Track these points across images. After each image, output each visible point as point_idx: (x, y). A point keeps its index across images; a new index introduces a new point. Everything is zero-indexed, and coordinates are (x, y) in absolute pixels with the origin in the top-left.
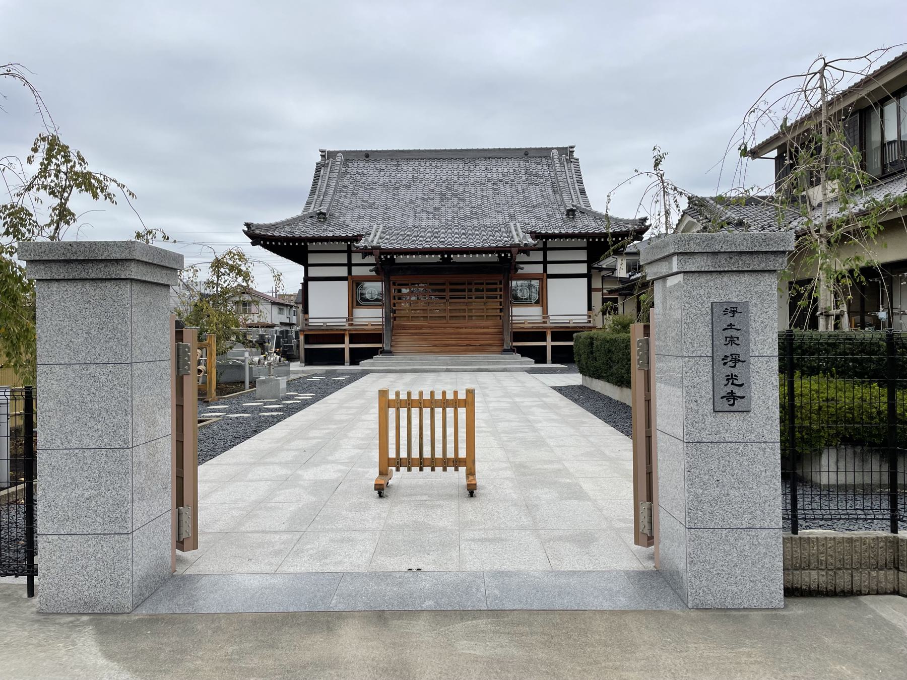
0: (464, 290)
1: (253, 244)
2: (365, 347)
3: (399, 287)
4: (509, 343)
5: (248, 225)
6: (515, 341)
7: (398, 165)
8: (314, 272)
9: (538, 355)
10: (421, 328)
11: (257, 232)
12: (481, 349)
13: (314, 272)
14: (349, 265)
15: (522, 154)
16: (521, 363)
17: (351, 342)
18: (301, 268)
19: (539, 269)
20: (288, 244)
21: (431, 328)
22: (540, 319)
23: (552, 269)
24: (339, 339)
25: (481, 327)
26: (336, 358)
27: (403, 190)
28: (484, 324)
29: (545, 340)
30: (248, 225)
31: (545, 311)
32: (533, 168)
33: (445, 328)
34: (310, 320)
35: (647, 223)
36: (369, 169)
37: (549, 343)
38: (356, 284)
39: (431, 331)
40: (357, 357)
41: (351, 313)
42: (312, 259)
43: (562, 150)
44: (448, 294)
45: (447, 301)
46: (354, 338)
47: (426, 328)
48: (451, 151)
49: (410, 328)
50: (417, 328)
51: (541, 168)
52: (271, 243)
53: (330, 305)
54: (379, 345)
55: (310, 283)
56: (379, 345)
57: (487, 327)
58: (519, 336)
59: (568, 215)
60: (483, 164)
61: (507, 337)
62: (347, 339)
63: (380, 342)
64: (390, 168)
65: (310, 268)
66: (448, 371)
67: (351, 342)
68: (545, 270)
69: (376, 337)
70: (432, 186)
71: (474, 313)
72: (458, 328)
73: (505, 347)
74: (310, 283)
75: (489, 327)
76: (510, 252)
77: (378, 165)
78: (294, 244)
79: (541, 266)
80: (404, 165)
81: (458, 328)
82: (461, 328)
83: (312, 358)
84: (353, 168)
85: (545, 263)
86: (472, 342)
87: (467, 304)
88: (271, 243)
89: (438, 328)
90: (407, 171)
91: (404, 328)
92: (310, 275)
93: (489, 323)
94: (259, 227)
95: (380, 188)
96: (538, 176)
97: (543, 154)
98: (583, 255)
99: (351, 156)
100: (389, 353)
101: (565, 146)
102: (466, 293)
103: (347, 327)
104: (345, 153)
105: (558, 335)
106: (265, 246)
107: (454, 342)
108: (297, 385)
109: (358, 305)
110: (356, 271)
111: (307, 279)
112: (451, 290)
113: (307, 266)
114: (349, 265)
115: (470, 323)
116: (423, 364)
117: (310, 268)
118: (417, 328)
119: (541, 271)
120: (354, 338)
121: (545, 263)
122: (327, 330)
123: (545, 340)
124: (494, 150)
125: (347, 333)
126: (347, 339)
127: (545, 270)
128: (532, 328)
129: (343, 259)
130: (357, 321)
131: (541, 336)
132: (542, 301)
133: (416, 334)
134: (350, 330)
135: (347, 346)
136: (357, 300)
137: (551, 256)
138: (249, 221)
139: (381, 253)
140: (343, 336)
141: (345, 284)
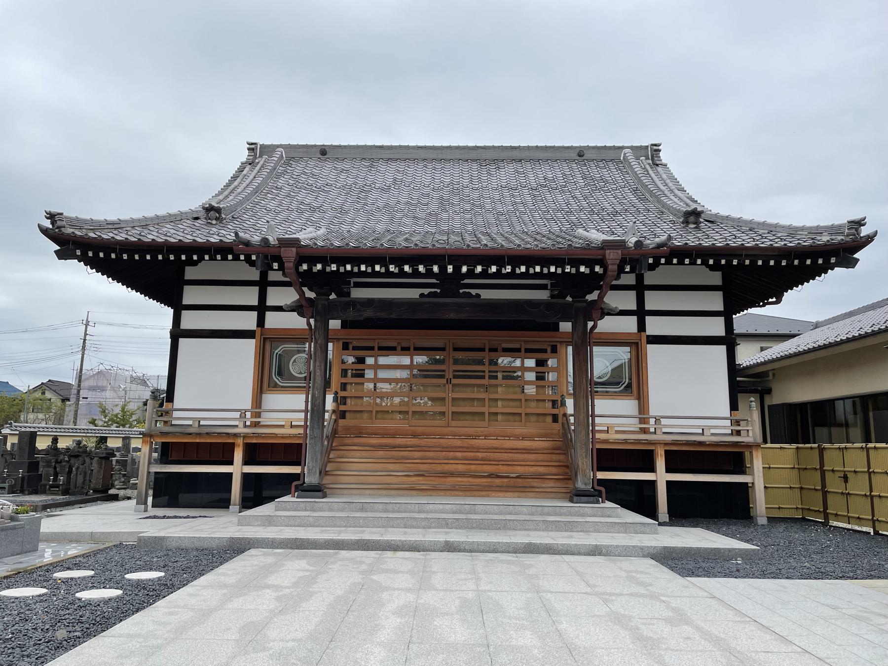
0: (480, 362)
1: (62, 255)
2: (273, 472)
3: (360, 353)
4: (588, 475)
5: (51, 216)
6: (600, 469)
7: (372, 166)
8: (190, 321)
9: (639, 499)
10: (393, 436)
11: (69, 231)
12: (520, 485)
13: (190, 321)
14: (262, 309)
15: (574, 155)
16: (626, 528)
17: (247, 462)
18: (168, 312)
19: (629, 324)
20: (131, 257)
21: (415, 435)
22: (633, 424)
23: (654, 326)
24: (224, 454)
25: (517, 438)
26: (211, 494)
27: (374, 195)
28: (519, 430)
29: (652, 469)
30: (51, 216)
31: (643, 408)
32: (595, 172)
33: (442, 436)
34: (176, 414)
35: (865, 231)
36: (327, 171)
37: (661, 476)
38: (268, 341)
39: (414, 441)
40: (258, 492)
41: (257, 402)
42: (191, 295)
43: (638, 150)
44: (450, 369)
45: (449, 381)
46: (254, 454)
47: (404, 435)
48: (458, 148)
49: (371, 434)
50: (384, 434)
51: (610, 173)
52: (96, 254)
53: (220, 387)
54: (296, 470)
55: (182, 341)
56: (296, 470)
57: (531, 438)
58: (609, 458)
59: (686, 222)
60: (510, 168)
61: (584, 462)
62: (238, 455)
63: (297, 463)
64: (359, 173)
65: (185, 314)
66: (450, 547)
67: (247, 462)
68: (642, 326)
69: (291, 452)
70: (426, 191)
71: (500, 407)
72: (469, 436)
73: (580, 485)
74: (182, 341)
75: (530, 439)
76: (602, 262)
77: (340, 166)
78: (143, 257)
79: (634, 319)
80: (382, 167)
81: (469, 436)
82: (476, 437)
83: (171, 493)
84: (298, 168)
85: (641, 313)
86: (503, 469)
87: (486, 388)
88: (96, 254)
89: (428, 435)
90: (387, 173)
91: (359, 433)
92: (185, 324)
93: (530, 428)
94: (76, 223)
95: (336, 191)
96: (606, 182)
97: (609, 155)
98: (716, 301)
99: (296, 154)
100: (317, 490)
101: (645, 144)
102: (486, 368)
103: (241, 430)
104: (288, 147)
105: (682, 457)
106: (88, 262)
107: (461, 468)
108: (109, 558)
109: (274, 387)
110: (273, 320)
111: (177, 334)
112: (456, 362)
113: (178, 308)
114: (262, 309)
115: (495, 428)
116: (388, 524)
117: (185, 314)
118: (384, 434)
119: (634, 329)
120: (254, 454)
121: (641, 313)
122: (199, 435)
123: (652, 469)
124: (529, 148)
125: (240, 441)
126: (238, 455)
127: (642, 326)
128: (626, 441)
129: (250, 296)
130: (267, 418)
131: (642, 459)
132: (632, 383)
133: (381, 447)
134: (245, 436)
135: (237, 469)
136: (269, 376)
137: (653, 301)
138: (54, 210)
139: (301, 259)
140: (231, 447)
141: (249, 346)
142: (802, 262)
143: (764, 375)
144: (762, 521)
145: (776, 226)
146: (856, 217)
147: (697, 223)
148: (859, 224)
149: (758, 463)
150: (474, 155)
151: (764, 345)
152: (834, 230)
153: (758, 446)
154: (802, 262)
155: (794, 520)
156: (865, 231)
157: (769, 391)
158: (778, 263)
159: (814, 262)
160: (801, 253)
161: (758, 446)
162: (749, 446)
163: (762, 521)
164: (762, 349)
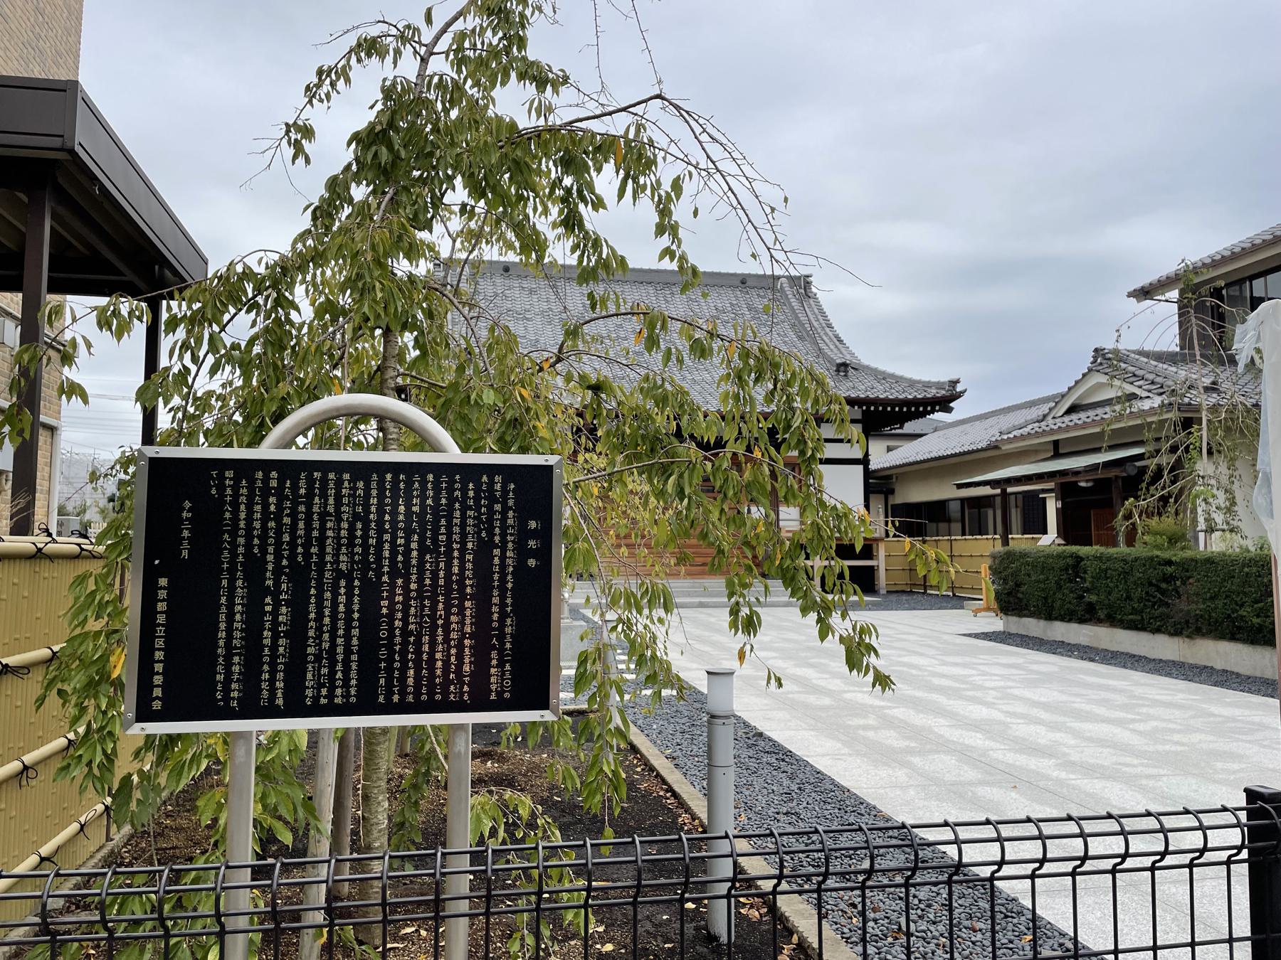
35: (959, 388)
59: (838, 371)
142: (909, 409)
143: (890, 477)
144: (883, 591)
145: (901, 378)
146: (954, 377)
147: (846, 372)
148: (954, 383)
149: (882, 551)
150: (647, 278)
151: (892, 443)
152: (939, 385)
153: (882, 540)
154: (909, 409)
155: (903, 592)
156: (959, 388)
157: (892, 492)
158: (893, 409)
159: (917, 409)
160: (916, 402)
161: (882, 540)
162: (876, 540)
163: (883, 591)
164: (889, 449)
